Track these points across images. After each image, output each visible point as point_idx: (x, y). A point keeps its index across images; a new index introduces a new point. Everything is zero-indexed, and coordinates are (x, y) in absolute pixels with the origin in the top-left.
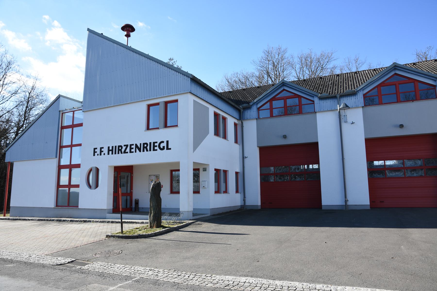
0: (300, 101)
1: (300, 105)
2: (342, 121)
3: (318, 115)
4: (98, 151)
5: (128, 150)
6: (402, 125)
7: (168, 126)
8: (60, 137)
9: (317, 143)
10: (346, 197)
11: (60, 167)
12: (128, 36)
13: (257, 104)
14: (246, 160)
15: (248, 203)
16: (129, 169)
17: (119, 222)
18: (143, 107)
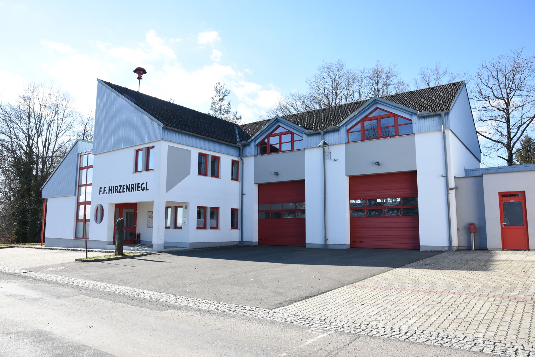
0: (396, 121)
1: (396, 125)
2: (327, 157)
3: (416, 136)
4: (102, 190)
5: (121, 190)
6: (378, 162)
7: (150, 168)
8: (78, 177)
9: (303, 182)
10: (325, 236)
11: (79, 204)
12: (140, 78)
13: (255, 141)
14: (244, 197)
15: (245, 240)
16: (134, 206)
17: (84, 251)
18: (131, 153)
